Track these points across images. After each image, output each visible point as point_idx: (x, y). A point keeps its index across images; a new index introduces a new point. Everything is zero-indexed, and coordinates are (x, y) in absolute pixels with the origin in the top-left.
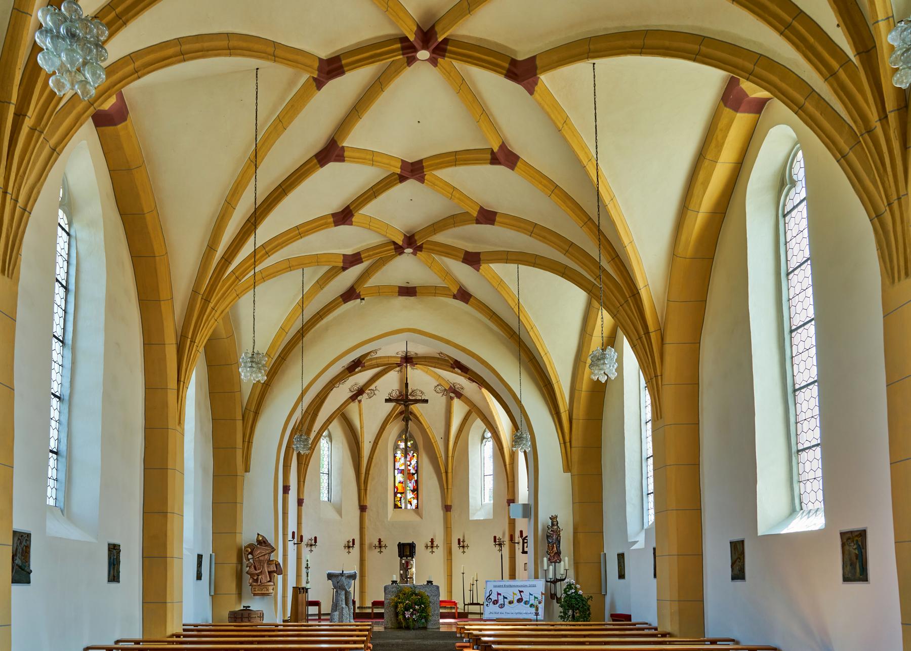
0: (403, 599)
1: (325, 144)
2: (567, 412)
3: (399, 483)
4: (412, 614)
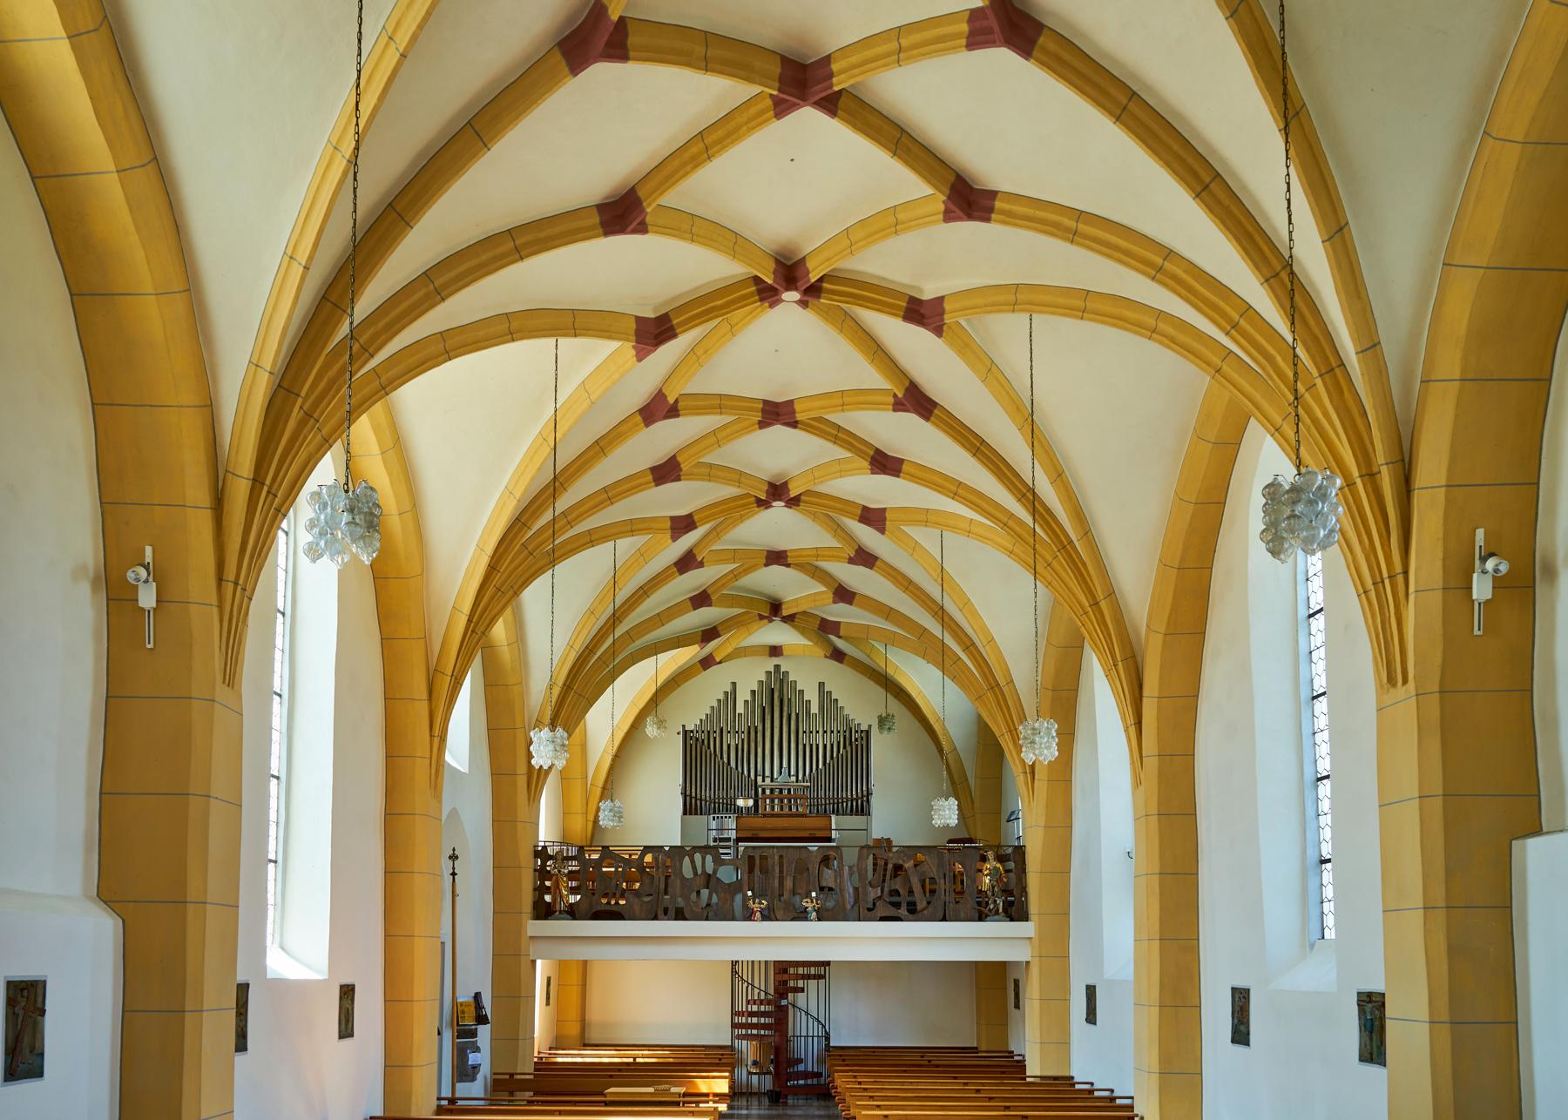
1: (607, 198)
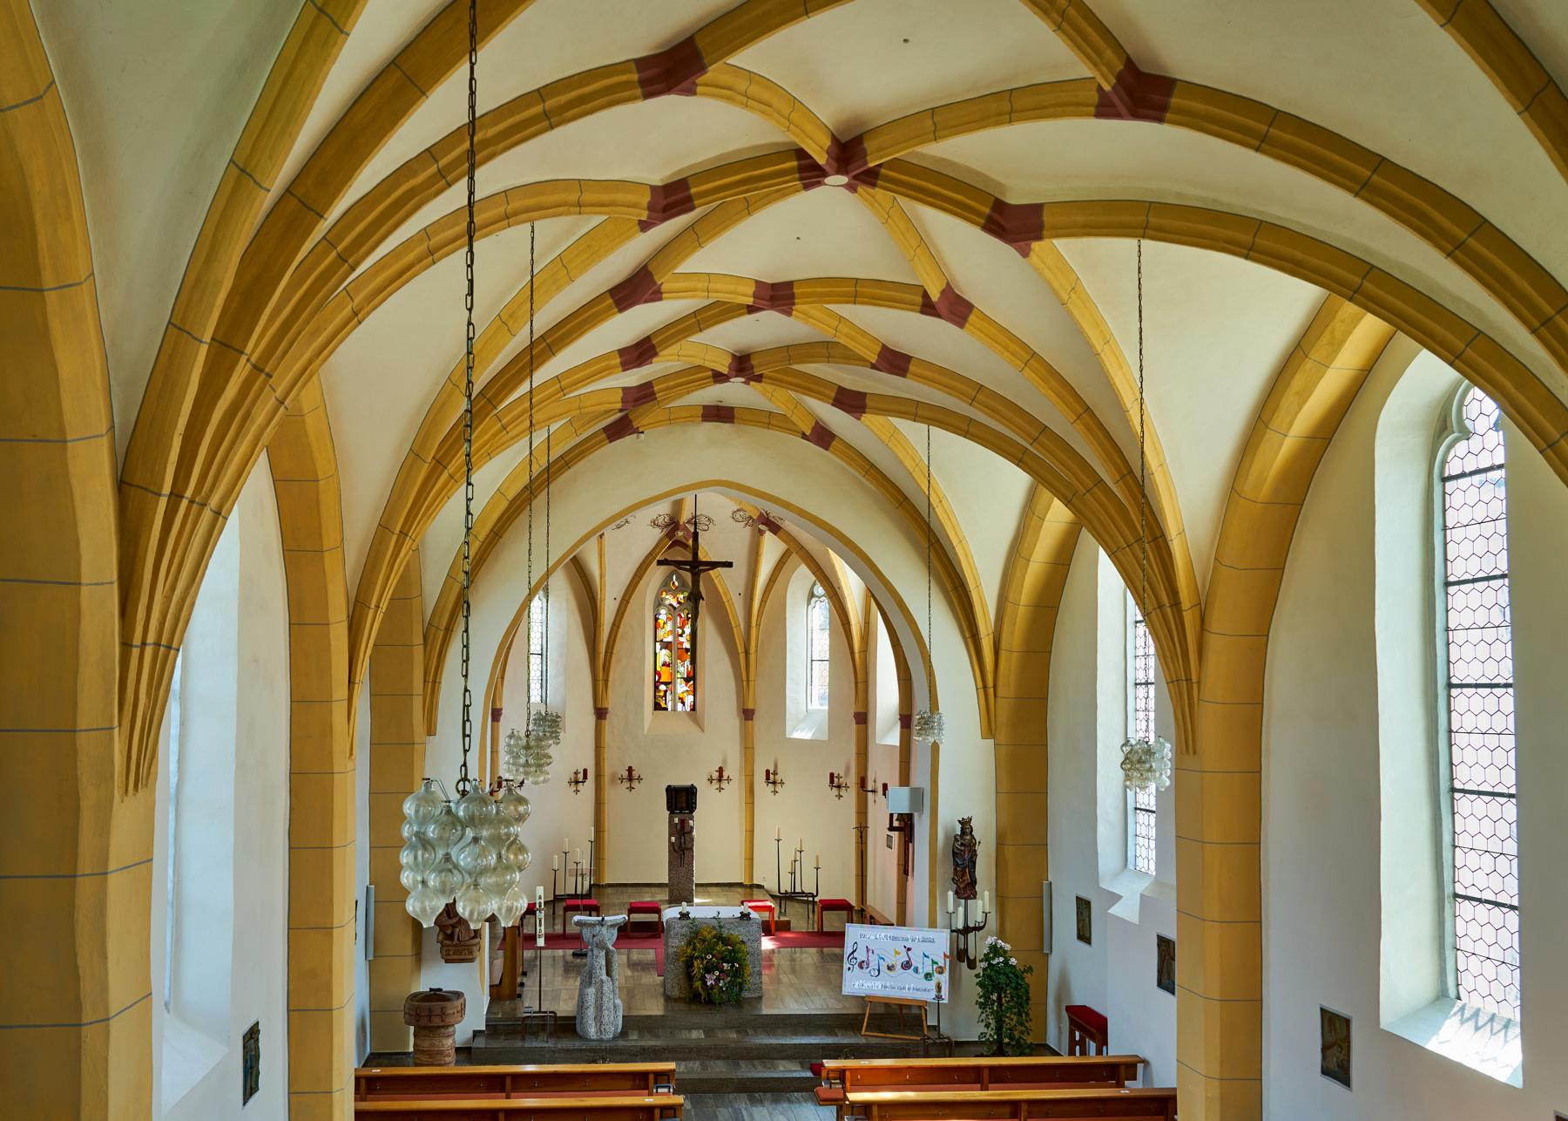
2: (991, 636)
4: (718, 979)
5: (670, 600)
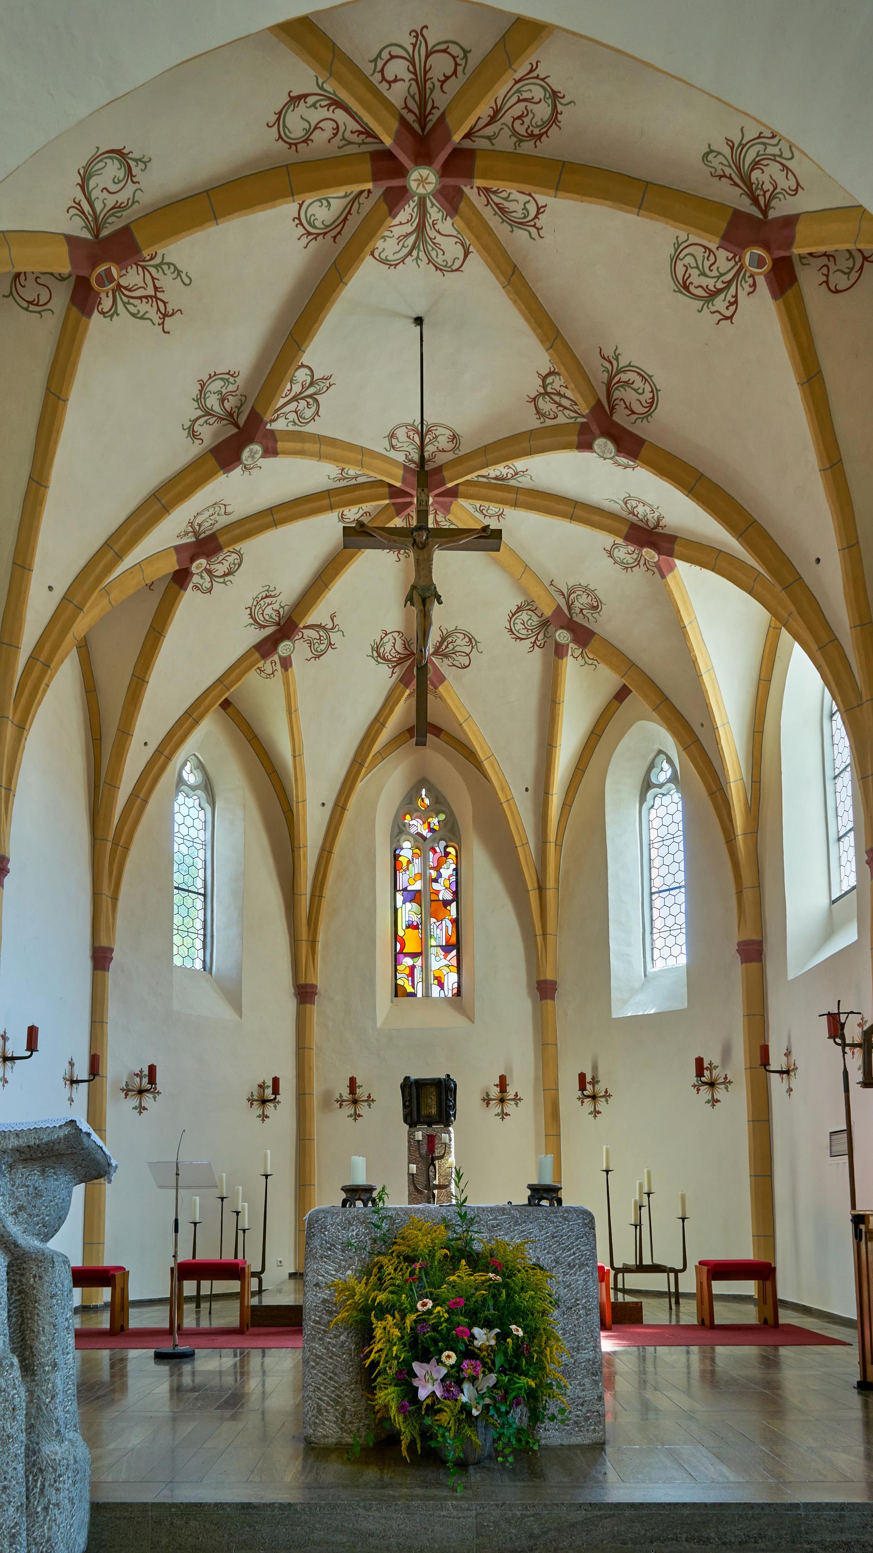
0: (397, 1291)
3: (408, 927)
5: (417, 826)
